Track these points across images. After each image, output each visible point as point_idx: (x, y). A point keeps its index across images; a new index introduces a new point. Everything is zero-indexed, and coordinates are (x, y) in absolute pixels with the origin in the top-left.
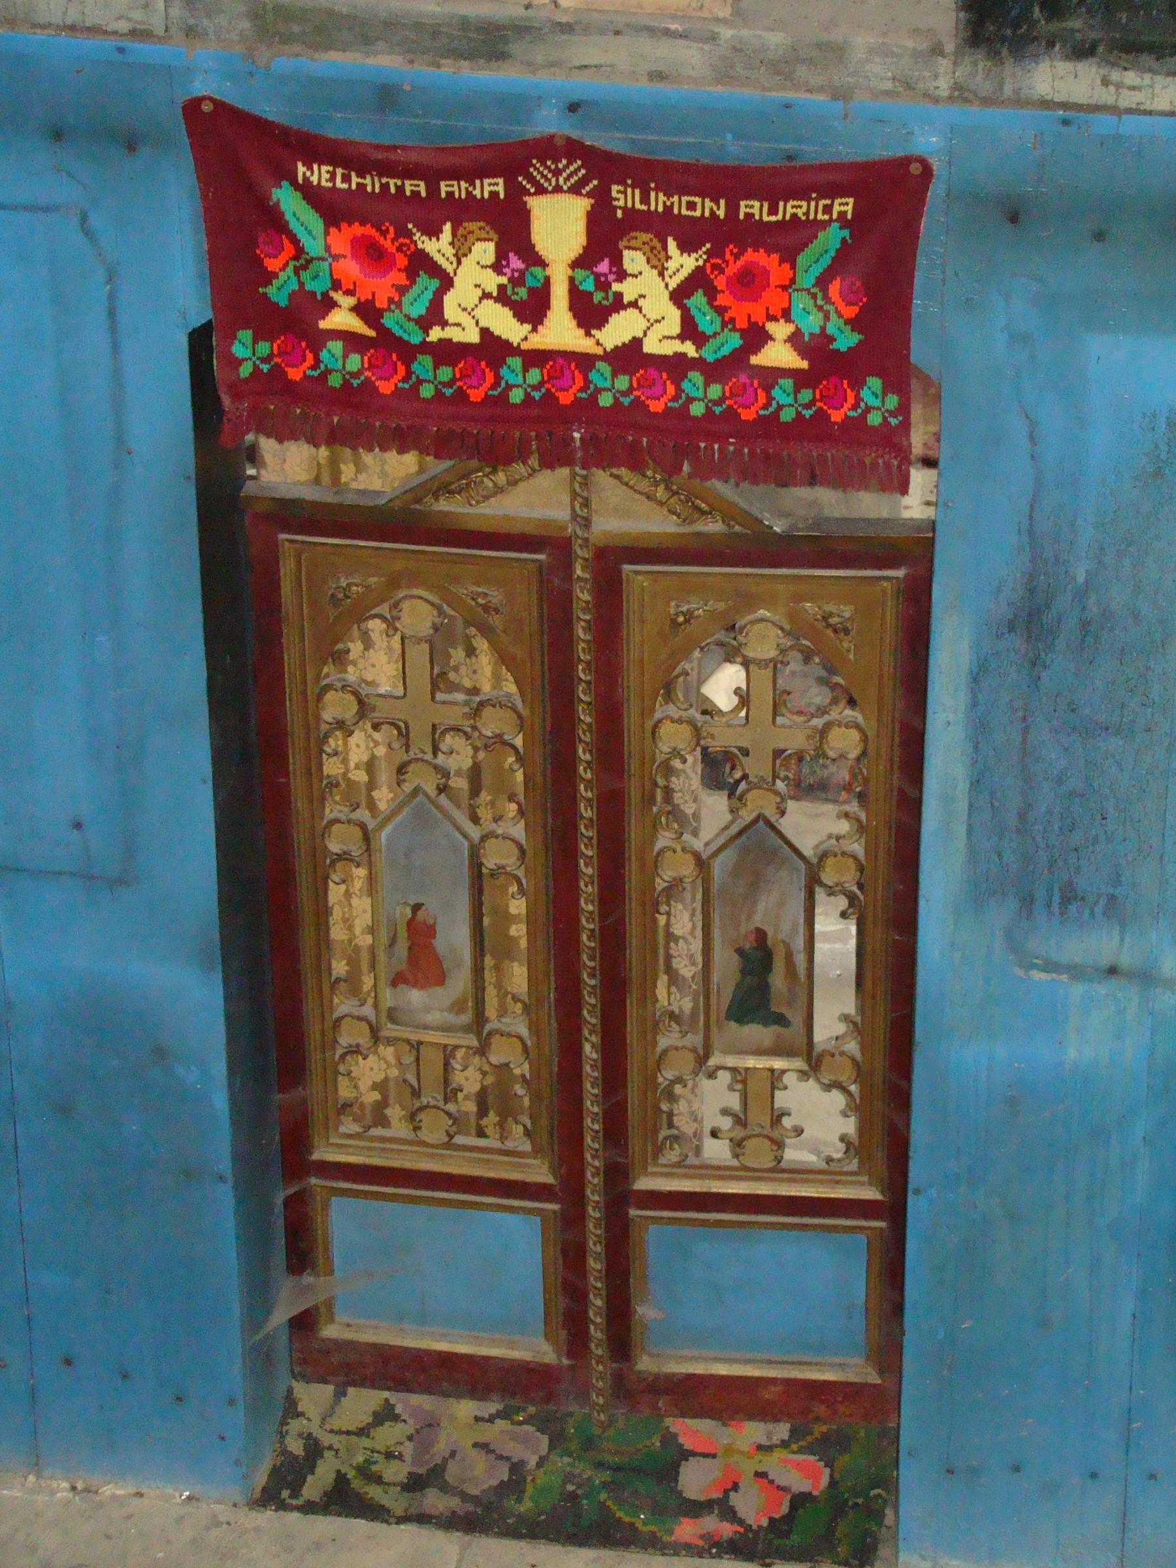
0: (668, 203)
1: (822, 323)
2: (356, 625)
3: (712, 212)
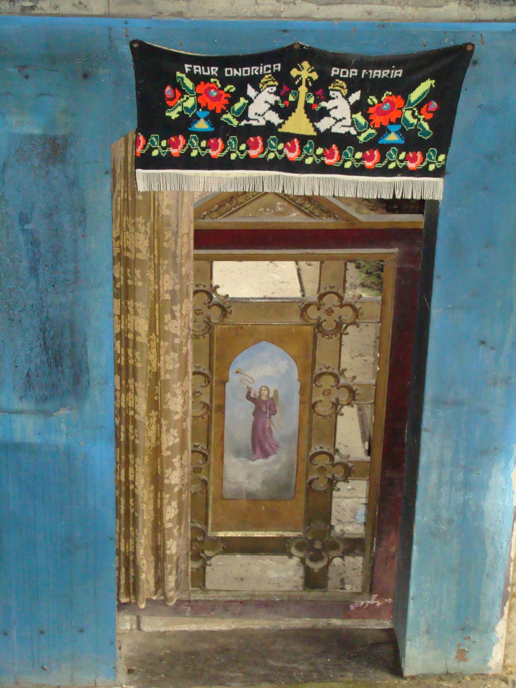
0: (367, 73)
1: (265, 111)
2: (280, 130)
3: (238, 71)
